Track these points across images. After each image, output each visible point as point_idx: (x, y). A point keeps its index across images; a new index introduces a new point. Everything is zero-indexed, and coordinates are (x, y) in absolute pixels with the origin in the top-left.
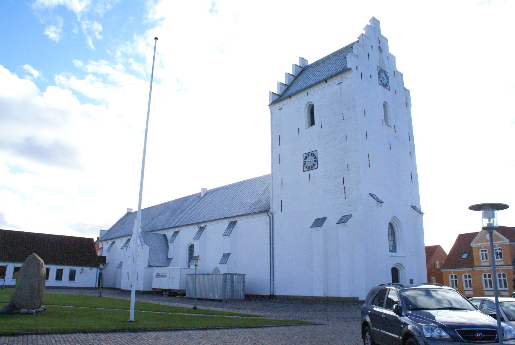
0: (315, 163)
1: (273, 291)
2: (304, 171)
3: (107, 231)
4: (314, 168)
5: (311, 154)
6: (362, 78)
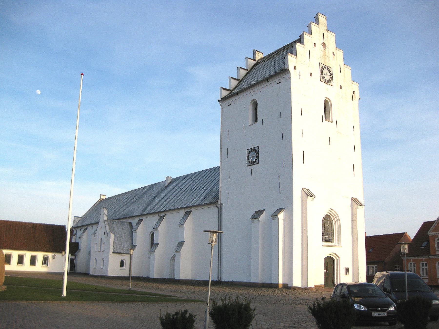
0: (256, 158)
1: (221, 277)
2: (247, 166)
3: (81, 217)
4: (256, 163)
5: (254, 149)
6: (280, 183)
